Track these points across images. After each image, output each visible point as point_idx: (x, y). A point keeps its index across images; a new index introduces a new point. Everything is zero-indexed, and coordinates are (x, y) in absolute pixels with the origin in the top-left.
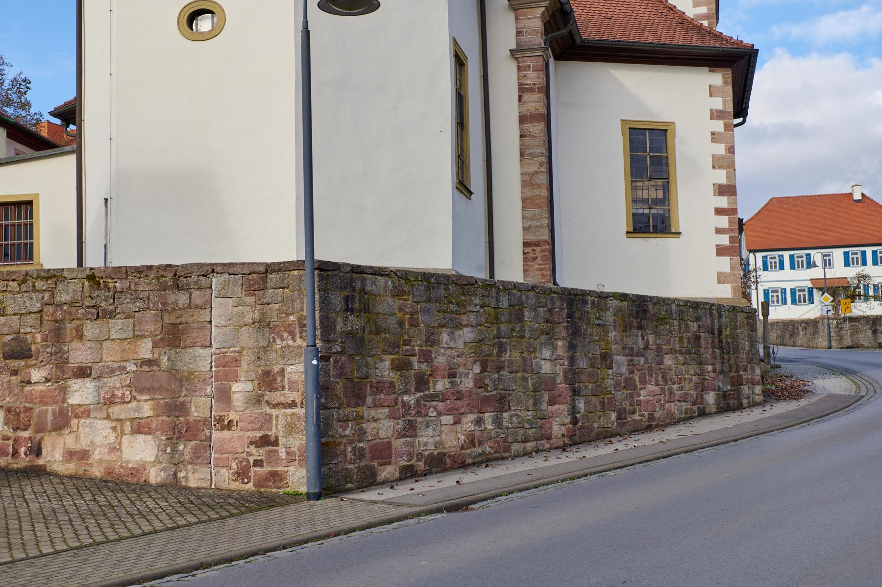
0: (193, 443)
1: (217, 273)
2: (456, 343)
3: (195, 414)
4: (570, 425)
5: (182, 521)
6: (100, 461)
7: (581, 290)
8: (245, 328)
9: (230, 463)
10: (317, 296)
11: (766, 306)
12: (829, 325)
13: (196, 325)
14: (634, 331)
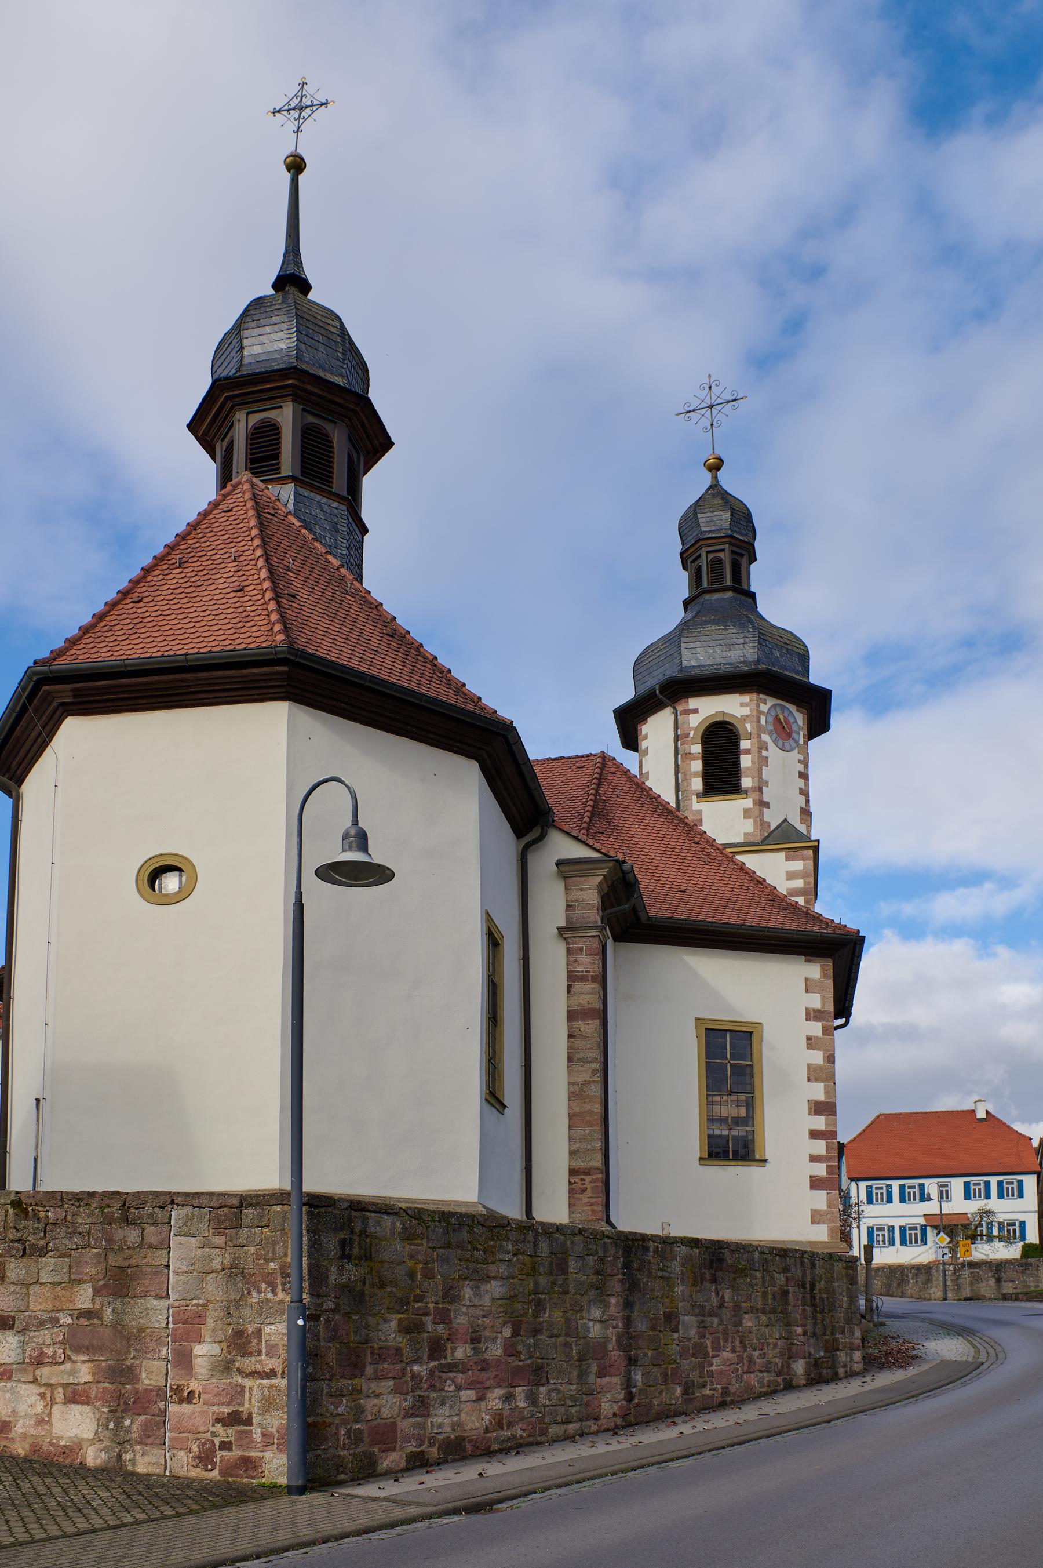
0: (143, 1417)
1: (178, 1205)
2: (482, 1300)
3: (146, 1382)
4: (624, 1402)
5: (127, 1518)
6: (24, 1436)
7: (641, 1234)
8: (211, 1275)
9: (190, 1444)
10: (305, 1239)
11: (869, 1250)
12: (944, 1271)
13: (149, 1270)
14: (707, 1284)
